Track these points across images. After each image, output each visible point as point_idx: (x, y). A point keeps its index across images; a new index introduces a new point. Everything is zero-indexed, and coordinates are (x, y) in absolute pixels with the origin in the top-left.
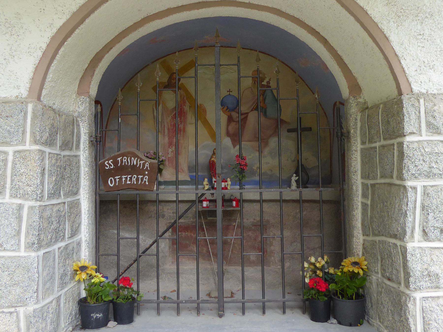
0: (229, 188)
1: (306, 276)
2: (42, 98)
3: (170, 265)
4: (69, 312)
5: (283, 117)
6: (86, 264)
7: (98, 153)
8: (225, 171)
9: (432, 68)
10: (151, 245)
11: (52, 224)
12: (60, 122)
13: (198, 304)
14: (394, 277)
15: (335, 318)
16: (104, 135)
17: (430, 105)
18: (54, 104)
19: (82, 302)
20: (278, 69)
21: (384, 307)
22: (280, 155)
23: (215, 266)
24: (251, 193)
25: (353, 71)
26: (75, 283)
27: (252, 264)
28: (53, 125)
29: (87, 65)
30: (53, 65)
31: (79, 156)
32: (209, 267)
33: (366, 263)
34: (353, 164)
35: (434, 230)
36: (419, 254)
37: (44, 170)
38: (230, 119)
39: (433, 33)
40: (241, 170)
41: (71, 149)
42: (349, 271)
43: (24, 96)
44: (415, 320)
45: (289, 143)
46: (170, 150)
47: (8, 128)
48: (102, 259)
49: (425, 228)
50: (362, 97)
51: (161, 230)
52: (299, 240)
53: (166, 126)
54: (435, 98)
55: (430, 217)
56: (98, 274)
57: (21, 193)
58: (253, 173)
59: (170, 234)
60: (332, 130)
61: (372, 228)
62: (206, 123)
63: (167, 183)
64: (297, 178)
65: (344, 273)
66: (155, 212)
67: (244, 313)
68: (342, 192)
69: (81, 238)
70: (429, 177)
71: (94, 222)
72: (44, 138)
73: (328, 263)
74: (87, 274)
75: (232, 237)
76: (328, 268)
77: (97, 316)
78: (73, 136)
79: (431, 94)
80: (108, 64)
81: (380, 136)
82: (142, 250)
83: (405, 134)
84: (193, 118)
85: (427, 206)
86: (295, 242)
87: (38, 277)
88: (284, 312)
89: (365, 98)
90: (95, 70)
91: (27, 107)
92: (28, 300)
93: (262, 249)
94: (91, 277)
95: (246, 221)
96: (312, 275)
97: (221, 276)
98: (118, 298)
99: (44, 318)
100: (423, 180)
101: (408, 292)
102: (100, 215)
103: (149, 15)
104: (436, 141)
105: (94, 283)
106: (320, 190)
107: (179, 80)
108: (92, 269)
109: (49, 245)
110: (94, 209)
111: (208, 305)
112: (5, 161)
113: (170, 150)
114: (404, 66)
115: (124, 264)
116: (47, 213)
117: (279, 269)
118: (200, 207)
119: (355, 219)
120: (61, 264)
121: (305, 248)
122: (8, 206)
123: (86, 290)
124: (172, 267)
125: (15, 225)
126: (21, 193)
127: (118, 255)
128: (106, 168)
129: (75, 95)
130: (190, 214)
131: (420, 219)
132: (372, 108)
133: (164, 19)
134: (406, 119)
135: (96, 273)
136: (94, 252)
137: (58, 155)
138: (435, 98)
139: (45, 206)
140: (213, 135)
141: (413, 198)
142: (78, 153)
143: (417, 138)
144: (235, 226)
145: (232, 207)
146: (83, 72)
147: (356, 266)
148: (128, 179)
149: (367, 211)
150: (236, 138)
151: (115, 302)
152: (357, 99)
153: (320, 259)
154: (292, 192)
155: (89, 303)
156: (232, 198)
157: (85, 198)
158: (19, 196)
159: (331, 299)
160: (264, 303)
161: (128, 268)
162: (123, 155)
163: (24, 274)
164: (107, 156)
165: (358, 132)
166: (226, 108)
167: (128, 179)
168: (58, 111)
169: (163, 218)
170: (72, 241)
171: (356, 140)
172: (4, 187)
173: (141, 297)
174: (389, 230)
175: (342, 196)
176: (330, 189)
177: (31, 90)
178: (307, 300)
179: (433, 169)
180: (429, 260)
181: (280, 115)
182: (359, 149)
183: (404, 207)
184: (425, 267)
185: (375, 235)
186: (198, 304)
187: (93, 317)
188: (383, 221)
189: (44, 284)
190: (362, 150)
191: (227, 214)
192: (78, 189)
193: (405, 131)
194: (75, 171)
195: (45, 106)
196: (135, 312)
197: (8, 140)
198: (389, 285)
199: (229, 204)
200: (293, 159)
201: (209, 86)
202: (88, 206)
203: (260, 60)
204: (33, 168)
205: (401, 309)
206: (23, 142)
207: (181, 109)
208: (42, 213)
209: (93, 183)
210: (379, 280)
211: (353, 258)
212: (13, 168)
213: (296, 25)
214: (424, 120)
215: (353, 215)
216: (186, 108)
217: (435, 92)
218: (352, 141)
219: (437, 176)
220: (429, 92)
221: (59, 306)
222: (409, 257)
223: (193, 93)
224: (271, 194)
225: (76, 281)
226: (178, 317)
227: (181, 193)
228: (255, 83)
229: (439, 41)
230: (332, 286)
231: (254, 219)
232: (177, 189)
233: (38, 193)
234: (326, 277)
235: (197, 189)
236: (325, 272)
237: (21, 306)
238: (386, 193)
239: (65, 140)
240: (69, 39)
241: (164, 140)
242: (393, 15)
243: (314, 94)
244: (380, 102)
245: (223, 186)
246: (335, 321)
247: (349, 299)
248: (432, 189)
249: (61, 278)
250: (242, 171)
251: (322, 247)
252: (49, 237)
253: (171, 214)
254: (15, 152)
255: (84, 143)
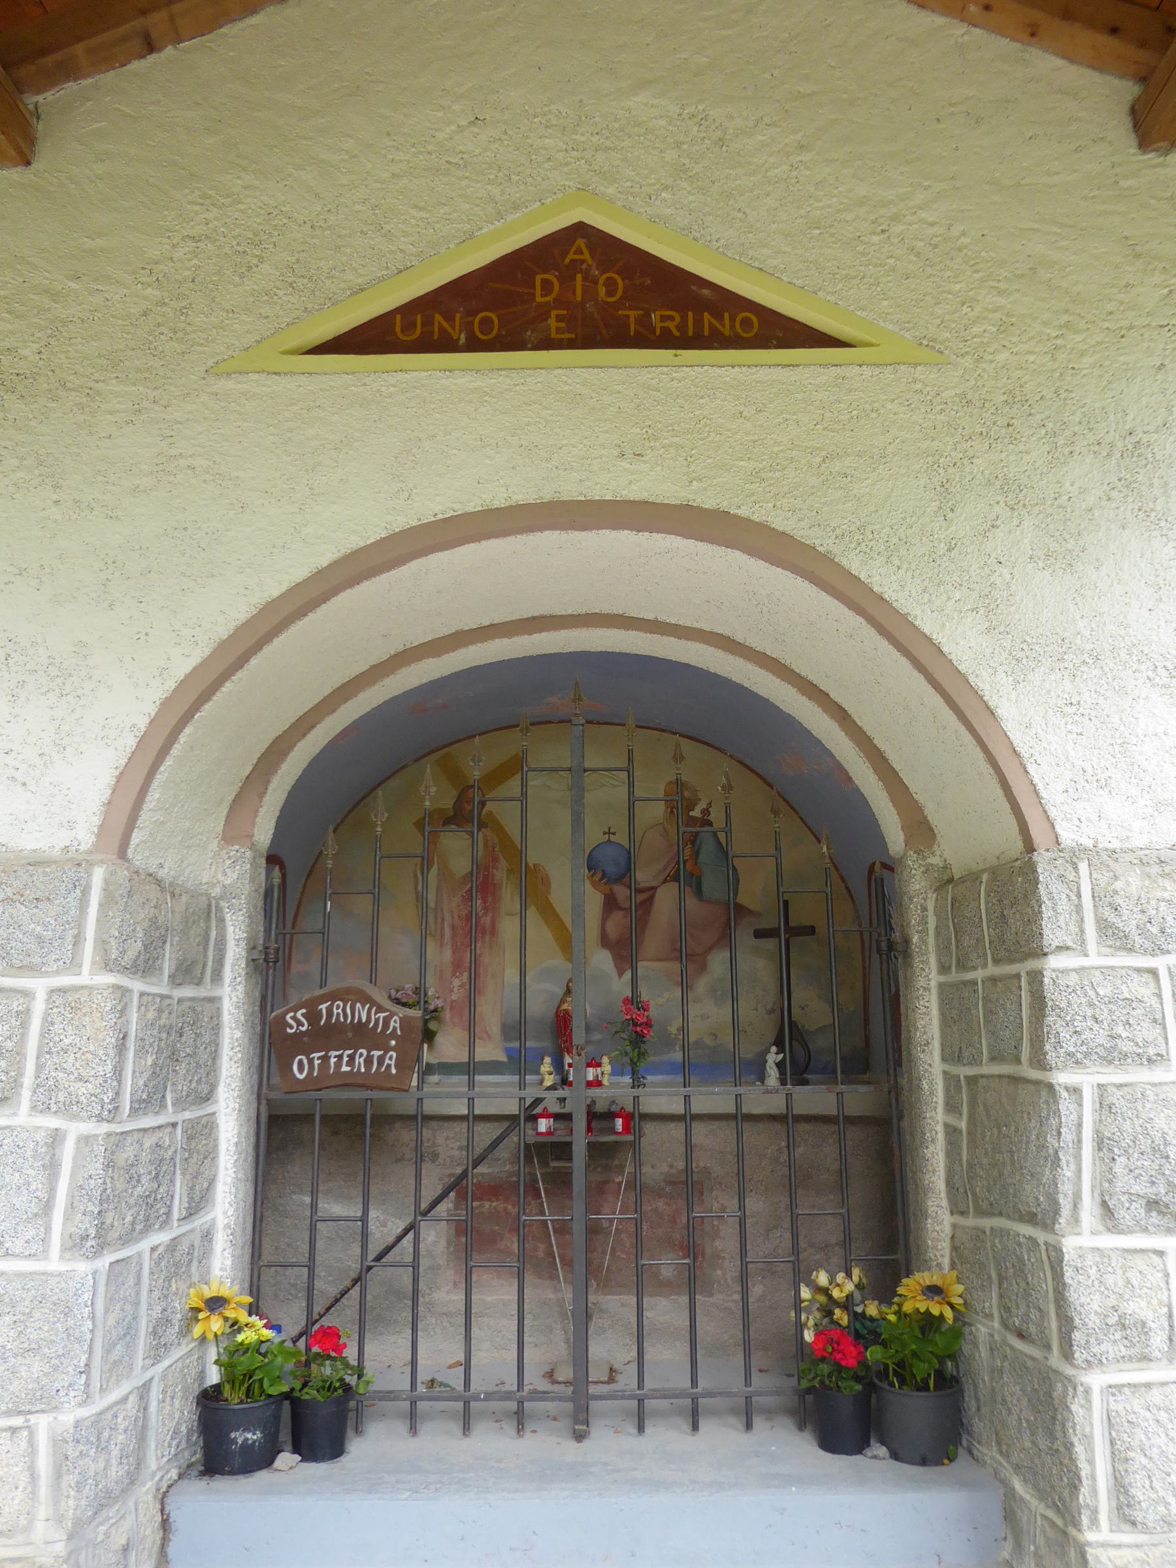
0: (605, 1082)
1: (806, 1324)
2: (130, 854)
3: (448, 1292)
4: (171, 1425)
5: (742, 899)
6: (225, 1292)
7: (270, 992)
8: (597, 1036)
9: (1104, 785)
10: (400, 1238)
11: (138, 1181)
12: (173, 912)
13: (521, 1403)
14: (1033, 1329)
15: (883, 1443)
16: (287, 942)
17: (1103, 878)
18: (161, 866)
19: (209, 1398)
20: (728, 780)
21: (1010, 1413)
22: (734, 999)
23: (568, 1294)
24: (662, 1096)
25: (913, 789)
26: (192, 1345)
27: (665, 1287)
28: (154, 921)
29: (249, 769)
30: (162, 769)
31: (220, 999)
32: (550, 1296)
33: (960, 1288)
34: (920, 1024)
35: (1131, 1201)
36: (1094, 1268)
37: (124, 1038)
38: (610, 903)
39: (1101, 701)
40: (635, 1035)
41: (199, 982)
42: (917, 1309)
43: (83, 847)
44: (1090, 1449)
45: (757, 964)
46: (456, 982)
47: (38, 929)
48: (268, 1275)
49: (1107, 1198)
50: (938, 853)
51: (429, 1193)
52: (787, 1224)
53: (448, 919)
54: (1116, 860)
55: (1119, 1167)
56: (254, 1319)
57: (62, 1099)
58: (667, 1042)
59: (451, 1206)
60: (866, 936)
61: (974, 1194)
62: (549, 913)
63: (446, 1068)
64: (781, 1056)
65: (906, 1315)
66: (413, 1144)
67: (641, 1429)
68: (893, 1094)
69: (213, 1219)
70: (1110, 1062)
71: (251, 1175)
72: (131, 954)
73: (864, 1288)
74: (226, 1319)
75: (614, 1214)
76: (863, 1302)
77: (247, 1439)
78: (206, 949)
79: (1106, 850)
80: (304, 765)
81: (985, 955)
82: (374, 1250)
83: (1046, 950)
84: (517, 898)
85: (1109, 1139)
86: (776, 1228)
87: (92, 1331)
88: (749, 1426)
89: (946, 855)
90: (268, 782)
91: (90, 875)
92: (61, 1393)
93: (691, 1249)
94: (236, 1327)
95: (651, 1171)
96: (821, 1320)
97: (582, 1321)
98: (305, 1385)
99: (103, 1444)
100: (1095, 1069)
101: (1069, 1371)
102: (268, 1152)
103: (408, 646)
104: (1122, 968)
105: (242, 1344)
106: (838, 1090)
107: (483, 804)
108: (239, 1304)
109: (126, 1239)
110: (252, 1139)
111: (549, 1405)
112: (24, 1016)
113: (456, 982)
114: (1036, 780)
115: (326, 1288)
116: (128, 1153)
117: (735, 1301)
118: (530, 1132)
119: (930, 1169)
120: (157, 1294)
121: (802, 1245)
122: (24, 1135)
123: (220, 1366)
124: (454, 1297)
125: (40, 1186)
126: (62, 1099)
127: (311, 1266)
128: (289, 1031)
129: (216, 842)
130: (504, 1152)
131: (1094, 1172)
132: (963, 880)
133: (446, 658)
134: (1047, 912)
135: (250, 1315)
136: (247, 1258)
137: (163, 997)
138: (1116, 860)
139: (122, 1133)
140: (565, 943)
141: (1074, 1117)
142: (217, 993)
143: (1074, 960)
144: (620, 1184)
145: (612, 1133)
146: (240, 784)
147: (936, 1298)
148: (346, 1059)
149: (960, 1147)
150: (625, 951)
151: (298, 1398)
152: (924, 858)
153: (840, 1277)
154: (768, 1095)
155: (226, 1400)
156: (614, 1108)
157: (229, 1111)
158: (54, 1108)
159: (870, 1387)
160: (695, 1400)
161: (337, 1300)
162: (333, 997)
163: (54, 1323)
164: (293, 1001)
165: (931, 940)
166: (599, 875)
167: (346, 1059)
168: (171, 884)
169: (433, 1161)
170: (187, 1227)
171: (927, 962)
172: (16, 1084)
173: (368, 1383)
174: (1016, 1200)
175: (894, 1106)
176: (863, 1089)
177: (102, 831)
178: (809, 1391)
179: (1119, 1041)
180: (1121, 1283)
181: (736, 894)
182: (933, 984)
183: (1051, 1140)
184: (1112, 1301)
185: (981, 1213)
186: (521, 1403)
187: (234, 1441)
188: (1001, 1174)
189: (108, 1349)
190: (941, 986)
191: (600, 1153)
192: (213, 1087)
193: (1045, 943)
194: (207, 1038)
195: (137, 872)
196: (350, 1424)
197: (36, 960)
198: (1021, 1352)
199: (605, 1124)
200: (769, 1006)
201: (559, 818)
202: (236, 1131)
203: (682, 758)
204: (98, 1030)
205: (1054, 1418)
206: (73, 965)
207: (486, 877)
208: (113, 1153)
209: (254, 1069)
210: (996, 1337)
211: (926, 1274)
212: (45, 1032)
213: (771, 675)
214: (1092, 915)
215: (924, 1157)
216: (500, 874)
217: (1116, 844)
218: (917, 962)
219: (1129, 1060)
220: (1101, 846)
221: (145, 1409)
222: (1068, 1273)
223: (517, 839)
224: (714, 1098)
225: (194, 1340)
226: (467, 1440)
227: (481, 1095)
228: (672, 812)
229: (1117, 720)
230: (874, 1354)
231: (671, 1166)
232: (471, 1085)
233: (106, 1100)
234: (858, 1325)
235: (522, 1085)
236: (856, 1314)
237: (43, 1411)
238: (1005, 1100)
239: (185, 960)
240: (207, 707)
241: (440, 956)
242: (1005, 655)
243: (819, 842)
244: (982, 866)
245: (590, 1078)
246: (882, 1451)
247: (919, 1389)
248: (1119, 1093)
249: (154, 1333)
250: (638, 1040)
251: (846, 1242)
252: (129, 1219)
253: (456, 1153)
254: (52, 991)
255: (233, 965)
